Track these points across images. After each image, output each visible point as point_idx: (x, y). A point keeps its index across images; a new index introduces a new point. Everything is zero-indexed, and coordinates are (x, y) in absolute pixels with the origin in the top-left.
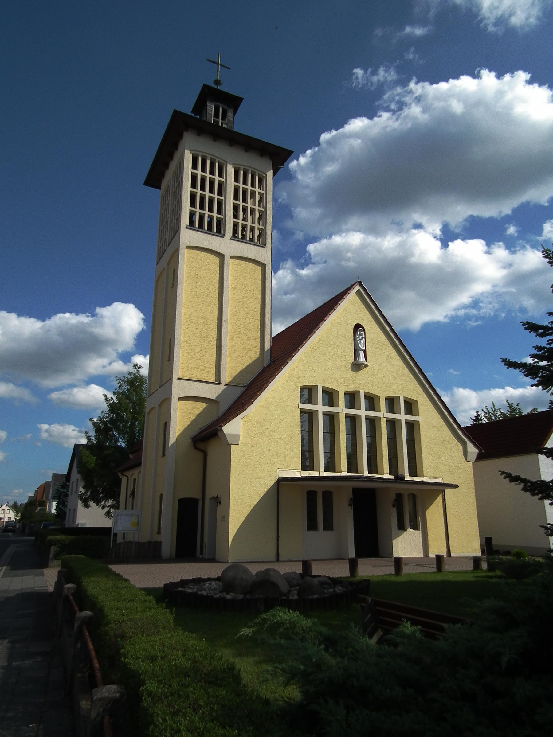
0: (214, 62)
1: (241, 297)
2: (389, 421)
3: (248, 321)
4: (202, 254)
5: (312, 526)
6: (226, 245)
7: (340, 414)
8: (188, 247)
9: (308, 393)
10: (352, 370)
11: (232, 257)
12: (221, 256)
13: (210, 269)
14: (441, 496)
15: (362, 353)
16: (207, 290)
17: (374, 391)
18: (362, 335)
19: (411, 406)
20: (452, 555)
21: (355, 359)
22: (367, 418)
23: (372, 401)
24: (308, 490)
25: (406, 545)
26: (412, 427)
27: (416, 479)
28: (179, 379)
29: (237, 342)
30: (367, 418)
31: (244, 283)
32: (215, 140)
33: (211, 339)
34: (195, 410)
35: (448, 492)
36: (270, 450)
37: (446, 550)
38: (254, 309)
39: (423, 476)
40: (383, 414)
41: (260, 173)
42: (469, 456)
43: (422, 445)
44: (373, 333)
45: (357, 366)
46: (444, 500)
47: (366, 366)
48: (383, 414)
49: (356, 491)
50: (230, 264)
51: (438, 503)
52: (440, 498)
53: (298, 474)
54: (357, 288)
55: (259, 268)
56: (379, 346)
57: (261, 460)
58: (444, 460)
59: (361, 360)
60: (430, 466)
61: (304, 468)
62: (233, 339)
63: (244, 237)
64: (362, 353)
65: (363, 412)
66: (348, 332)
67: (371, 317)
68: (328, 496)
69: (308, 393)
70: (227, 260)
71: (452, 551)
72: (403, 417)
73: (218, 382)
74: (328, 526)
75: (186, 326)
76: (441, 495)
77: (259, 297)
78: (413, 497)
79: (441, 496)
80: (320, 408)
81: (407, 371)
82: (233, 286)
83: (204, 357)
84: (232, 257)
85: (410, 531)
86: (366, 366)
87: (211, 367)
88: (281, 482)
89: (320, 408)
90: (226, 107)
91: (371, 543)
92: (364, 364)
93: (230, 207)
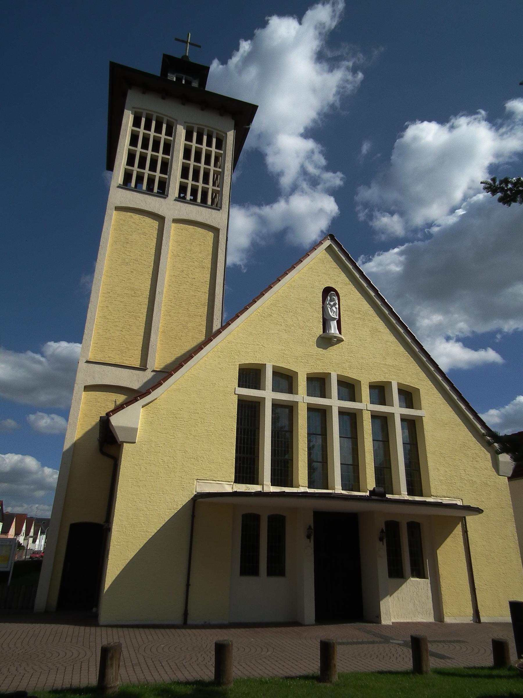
0: (183, 41)
1: (185, 266)
2: (375, 416)
3: (193, 293)
4: (137, 217)
5: (249, 567)
6: (169, 207)
7: (299, 404)
8: (118, 209)
9: (250, 376)
10: (318, 346)
11: (175, 221)
12: (160, 219)
13: (145, 234)
14: (459, 528)
15: (334, 324)
16: (139, 257)
17: (352, 374)
18: (334, 300)
19: (409, 396)
20: (483, 619)
21: (324, 330)
22: (342, 413)
23: (349, 388)
24: (410, 520)
25: (404, 605)
26: (412, 425)
27: (417, 498)
28: (88, 362)
29: (175, 318)
30: (342, 413)
31: (190, 250)
32: (163, 98)
33: (139, 314)
34: (108, 403)
35: (471, 520)
36: (186, 452)
37: (472, 612)
38: (202, 281)
39: (430, 496)
40: (365, 405)
41: (218, 132)
42: (501, 468)
43: (428, 451)
44: (350, 298)
45: (326, 341)
46: (465, 532)
47: (340, 340)
48: (365, 405)
49: (320, 517)
50: (172, 231)
51: (455, 537)
52: (458, 530)
53: (229, 487)
54: (328, 243)
55: (210, 235)
56: (360, 316)
57: (170, 466)
58: (462, 472)
59: (333, 332)
60: (441, 481)
61: (238, 480)
62: (170, 316)
63: (195, 199)
64: (334, 324)
65: (334, 402)
66: (314, 297)
67: (347, 279)
68: (277, 523)
69: (250, 376)
70: (168, 222)
71: (481, 614)
72: (397, 410)
73: (143, 368)
74: (277, 568)
75: (106, 297)
76: (460, 525)
77: (210, 266)
78: (414, 528)
79: (459, 528)
80: (268, 394)
81: (401, 349)
82: (175, 253)
83: (127, 336)
84: (175, 221)
85: (413, 581)
86: (340, 340)
87: (136, 348)
88: (199, 499)
89: (268, 394)
90: (189, 78)
91: (346, 598)
92: (335, 337)
93: (178, 166)
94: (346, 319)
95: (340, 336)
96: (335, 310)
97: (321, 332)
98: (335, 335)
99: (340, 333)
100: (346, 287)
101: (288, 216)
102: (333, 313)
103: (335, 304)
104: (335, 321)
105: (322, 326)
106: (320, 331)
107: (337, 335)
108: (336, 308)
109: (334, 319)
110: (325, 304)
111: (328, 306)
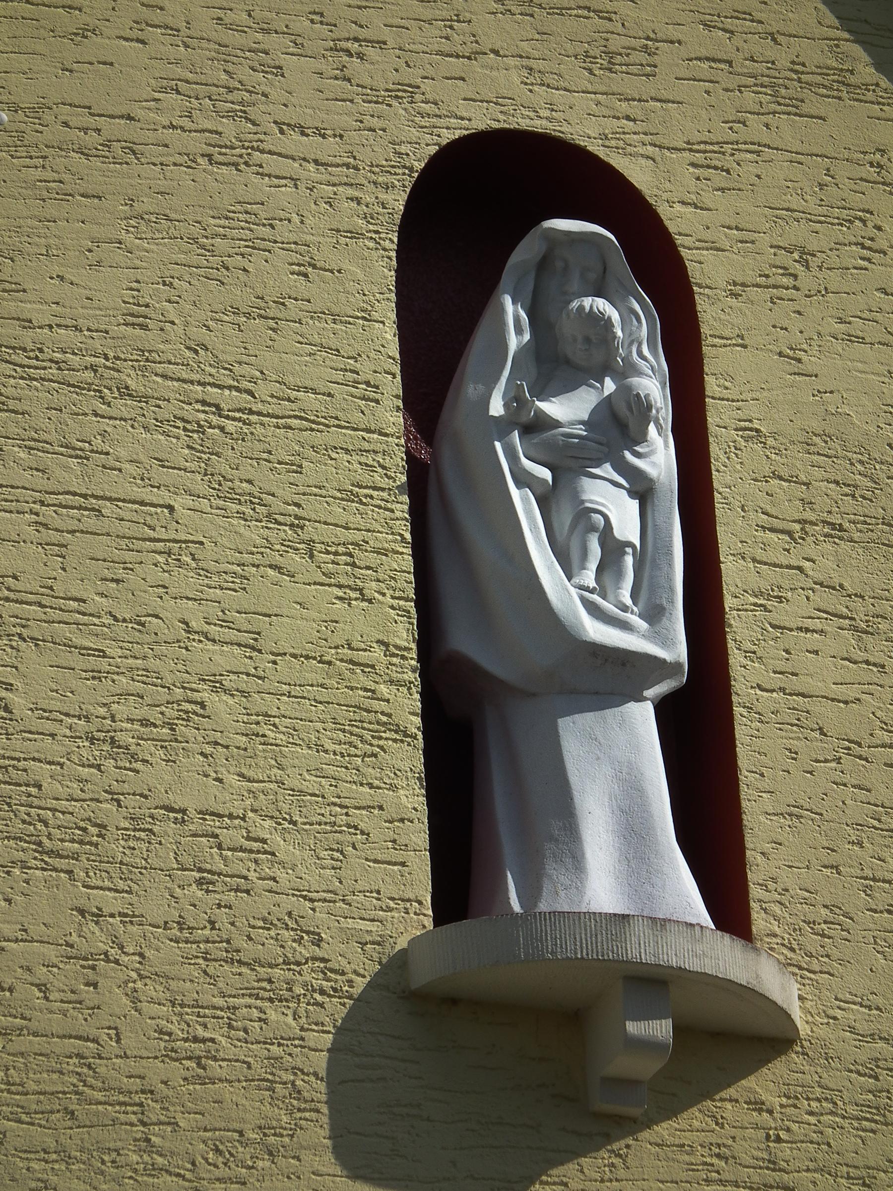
47: (731, 1039)
59: (601, 887)
64: (615, 763)
66: (267, 311)
92: (653, 985)
94: (822, 674)
95: (723, 957)
96: (624, 517)
97: (411, 919)
98: (642, 948)
99: (730, 909)
100: (788, 131)
101: (640, 384)
102: (589, 578)
103: (617, 428)
104: (642, 717)
105: (412, 799)
106: (380, 892)
107: (676, 953)
108: (642, 490)
109: (611, 676)
110: (457, 418)
111: (510, 455)
